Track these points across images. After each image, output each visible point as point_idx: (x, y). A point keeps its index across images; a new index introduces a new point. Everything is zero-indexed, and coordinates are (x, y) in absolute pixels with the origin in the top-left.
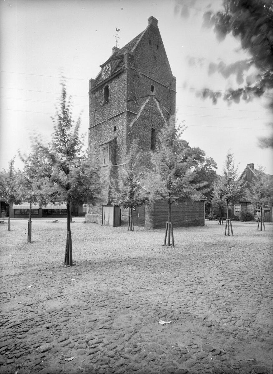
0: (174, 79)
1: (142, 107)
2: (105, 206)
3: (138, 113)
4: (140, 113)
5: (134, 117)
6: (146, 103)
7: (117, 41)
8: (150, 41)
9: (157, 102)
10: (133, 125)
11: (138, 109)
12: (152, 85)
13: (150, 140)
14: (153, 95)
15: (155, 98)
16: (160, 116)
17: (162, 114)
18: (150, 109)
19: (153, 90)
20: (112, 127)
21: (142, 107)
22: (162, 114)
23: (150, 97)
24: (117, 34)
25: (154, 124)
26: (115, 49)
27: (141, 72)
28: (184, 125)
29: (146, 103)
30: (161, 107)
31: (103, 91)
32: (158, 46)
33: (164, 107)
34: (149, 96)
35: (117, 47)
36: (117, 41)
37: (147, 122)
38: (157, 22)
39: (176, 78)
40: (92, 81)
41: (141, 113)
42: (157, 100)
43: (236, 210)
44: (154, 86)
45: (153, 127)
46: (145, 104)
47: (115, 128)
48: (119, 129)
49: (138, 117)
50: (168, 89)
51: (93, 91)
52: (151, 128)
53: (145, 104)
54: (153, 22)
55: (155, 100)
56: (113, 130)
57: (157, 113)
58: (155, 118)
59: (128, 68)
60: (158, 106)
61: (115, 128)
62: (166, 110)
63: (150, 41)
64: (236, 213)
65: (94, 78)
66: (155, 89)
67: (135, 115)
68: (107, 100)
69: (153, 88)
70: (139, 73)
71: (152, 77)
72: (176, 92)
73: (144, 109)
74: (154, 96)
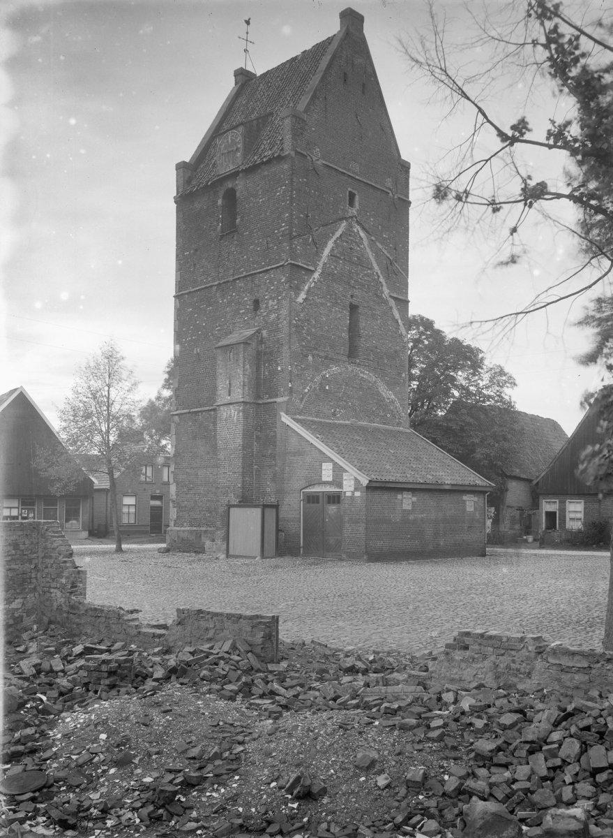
0: (405, 167)
1: (327, 251)
2: (234, 506)
3: (316, 266)
4: (321, 264)
5: (306, 277)
6: (334, 238)
7: (246, 51)
8: (345, 74)
9: (362, 234)
10: (305, 300)
11: (318, 255)
12: (349, 189)
13: (345, 335)
14: (352, 217)
15: (359, 223)
16: (371, 268)
17: (375, 265)
18: (346, 252)
19: (351, 203)
20: (248, 299)
21: (327, 251)
22: (375, 265)
23: (344, 224)
24: (247, 33)
25: (357, 292)
26: (243, 77)
27: (324, 159)
28: (386, 698)
29: (334, 238)
30: (372, 243)
31: (220, 202)
32: (364, 85)
33: (378, 244)
34: (341, 219)
35: (247, 69)
36: (246, 51)
37: (338, 288)
38: (363, 22)
39: (409, 164)
40: (181, 167)
41: (325, 264)
42: (364, 229)
43: (572, 515)
44: (356, 192)
45: (354, 301)
46: (333, 240)
47: (257, 303)
48: (267, 307)
49: (316, 275)
50: (391, 194)
51: (184, 199)
52: (348, 303)
53: (333, 240)
54: (352, 20)
55: (357, 228)
56: (250, 306)
57: (362, 263)
58: (358, 274)
59: (293, 153)
60: (366, 242)
61: (257, 303)
62: (386, 252)
63: (345, 74)
64: (572, 523)
65: (187, 158)
66: (357, 198)
67: (313, 272)
68: (231, 229)
69: (352, 196)
70: (319, 162)
71: (349, 170)
72: (410, 203)
73: (332, 255)
74: (356, 218)
